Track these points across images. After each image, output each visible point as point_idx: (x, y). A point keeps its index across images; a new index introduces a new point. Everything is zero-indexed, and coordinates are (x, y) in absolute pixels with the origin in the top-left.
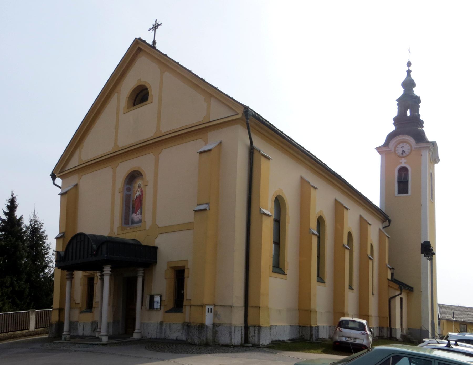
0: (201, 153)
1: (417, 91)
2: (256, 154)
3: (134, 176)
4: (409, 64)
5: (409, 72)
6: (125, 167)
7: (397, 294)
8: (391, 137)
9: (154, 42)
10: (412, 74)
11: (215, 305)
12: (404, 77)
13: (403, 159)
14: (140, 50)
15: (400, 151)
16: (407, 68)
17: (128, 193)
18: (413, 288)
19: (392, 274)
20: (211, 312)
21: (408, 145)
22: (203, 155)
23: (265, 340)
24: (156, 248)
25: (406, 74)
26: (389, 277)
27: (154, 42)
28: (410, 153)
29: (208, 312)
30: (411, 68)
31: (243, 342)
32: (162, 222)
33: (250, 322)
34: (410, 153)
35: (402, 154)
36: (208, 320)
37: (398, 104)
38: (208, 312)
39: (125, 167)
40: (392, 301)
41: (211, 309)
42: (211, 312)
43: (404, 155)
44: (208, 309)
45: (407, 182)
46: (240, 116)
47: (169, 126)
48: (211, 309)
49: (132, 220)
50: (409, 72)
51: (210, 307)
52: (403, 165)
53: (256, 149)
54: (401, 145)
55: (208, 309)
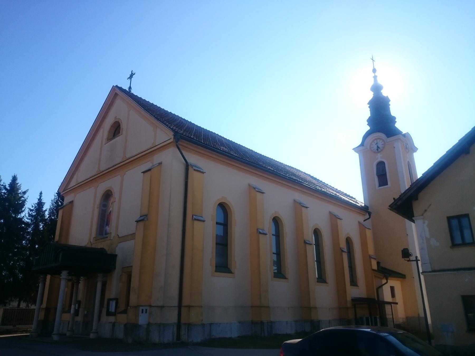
0: (144, 172)
1: (385, 93)
2: (191, 170)
3: (108, 195)
4: (374, 71)
5: (375, 77)
6: (103, 187)
7: (383, 283)
8: (368, 135)
9: (130, 88)
10: (378, 78)
11: (151, 306)
12: (372, 83)
13: (379, 154)
14: (116, 95)
15: (375, 147)
16: (373, 75)
17: (104, 209)
18: (405, 275)
19: (378, 263)
20: (146, 312)
21: (381, 141)
22: (146, 173)
23: (197, 337)
24: (117, 255)
25: (373, 79)
26: (375, 266)
27: (130, 88)
28: (384, 148)
29: (142, 312)
30: (376, 74)
31: (175, 339)
32: (122, 233)
33: (183, 321)
34: (384, 148)
35: (377, 149)
36: (143, 320)
37: (369, 107)
38: (142, 312)
39: (103, 187)
40: (380, 290)
41: (146, 310)
42: (146, 312)
43: (379, 150)
44: (143, 310)
45: (385, 174)
46: (172, 140)
47: (132, 152)
48: (146, 310)
49: (106, 231)
50: (375, 77)
51: (144, 308)
52: (380, 160)
53: (192, 166)
54: (376, 142)
55: (143, 310)
